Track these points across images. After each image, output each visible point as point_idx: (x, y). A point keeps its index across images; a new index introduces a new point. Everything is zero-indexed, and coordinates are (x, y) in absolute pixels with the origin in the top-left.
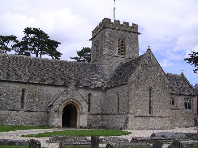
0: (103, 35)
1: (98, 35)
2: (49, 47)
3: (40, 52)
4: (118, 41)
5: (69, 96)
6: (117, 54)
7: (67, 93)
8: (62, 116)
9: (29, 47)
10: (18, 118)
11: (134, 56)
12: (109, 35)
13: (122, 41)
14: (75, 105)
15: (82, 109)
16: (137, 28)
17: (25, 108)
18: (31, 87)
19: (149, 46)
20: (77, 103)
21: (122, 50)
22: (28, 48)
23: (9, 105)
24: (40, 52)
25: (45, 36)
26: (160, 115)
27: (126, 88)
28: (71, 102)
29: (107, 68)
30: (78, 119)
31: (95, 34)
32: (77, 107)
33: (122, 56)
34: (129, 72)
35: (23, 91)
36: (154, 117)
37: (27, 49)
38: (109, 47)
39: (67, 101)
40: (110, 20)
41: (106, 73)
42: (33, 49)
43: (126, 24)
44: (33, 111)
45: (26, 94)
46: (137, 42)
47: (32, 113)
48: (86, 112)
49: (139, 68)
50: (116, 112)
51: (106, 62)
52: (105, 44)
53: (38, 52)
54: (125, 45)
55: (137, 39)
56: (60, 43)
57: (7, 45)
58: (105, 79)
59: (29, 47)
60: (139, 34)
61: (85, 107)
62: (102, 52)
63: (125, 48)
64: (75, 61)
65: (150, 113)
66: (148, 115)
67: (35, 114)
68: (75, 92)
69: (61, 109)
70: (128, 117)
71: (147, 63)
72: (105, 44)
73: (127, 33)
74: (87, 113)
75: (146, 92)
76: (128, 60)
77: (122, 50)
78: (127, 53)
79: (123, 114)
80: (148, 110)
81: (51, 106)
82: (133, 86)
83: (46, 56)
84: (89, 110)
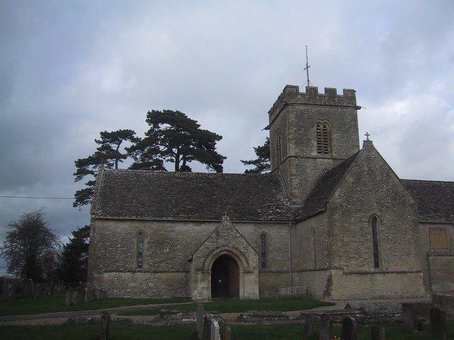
0: (284, 119)
1: (278, 120)
2: (199, 145)
3: (181, 156)
4: (315, 128)
5: (221, 242)
6: (314, 154)
7: (218, 235)
8: (210, 278)
9: (162, 148)
10: (133, 284)
11: (345, 155)
13: (324, 127)
14: (233, 256)
15: (248, 263)
16: (353, 98)
17: (146, 267)
19: (367, 135)
20: (238, 254)
21: (324, 144)
22: (160, 152)
23: (116, 262)
24: (181, 156)
25: (193, 125)
26: (399, 269)
27: (324, 219)
29: (296, 181)
30: (241, 282)
31: (273, 117)
32: (238, 261)
33: (326, 156)
34: (331, 189)
36: (384, 273)
37: (157, 151)
38: (300, 142)
39: (218, 251)
40: (297, 88)
41: (294, 191)
42: (169, 152)
43: (331, 92)
44: (160, 272)
47: (159, 274)
48: (254, 268)
49: (349, 179)
50: (311, 266)
51: (294, 171)
52: (291, 136)
53: (177, 158)
54: (330, 133)
55: (356, 116)
57: (118, 147)
58: (294, 203)
59: (162, 148)
60: (359, 108)
61: (253, 260)
62: (285, 153)
64: (253, 167)
65: (377, 265)
66: (372, 270)
67: (164, 276)
69: (209, 264)
70: (331, 276)
71: (366, 168)
72: (291, 136)
74: (256, 272)
75: (366, 225)
76: (339, 163)
77: (324, 144)
78: (335, 149)
79: (323, 270)
80: (372, 259)
81: (190, 261)
82: (337, 217)
83: (197, 167)
84: (264, 264)
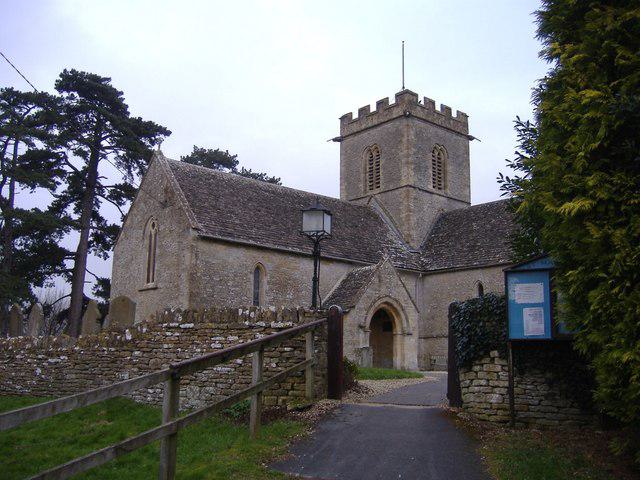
5: (384, 290)
6: (430, 187)
12: (417, 135)
15: (408, 321)
18: (277, 259)
20: (399, 308)
28: (386, 303)
35: (258, 270)
38: (418, 169)
43: (447, 110)
45: (265, 280)
46: (468, 160)
56: (167, 133)
60: (471, 138)
63: (445, 172)
68: (395, 279)
73: (448, 134)
